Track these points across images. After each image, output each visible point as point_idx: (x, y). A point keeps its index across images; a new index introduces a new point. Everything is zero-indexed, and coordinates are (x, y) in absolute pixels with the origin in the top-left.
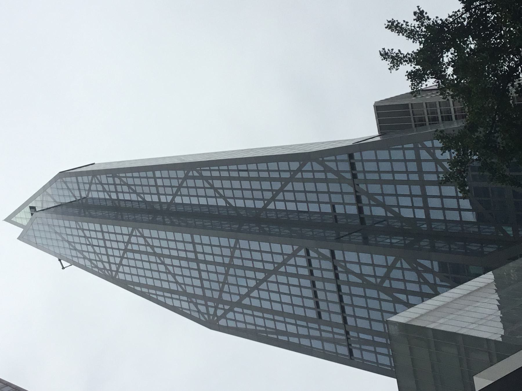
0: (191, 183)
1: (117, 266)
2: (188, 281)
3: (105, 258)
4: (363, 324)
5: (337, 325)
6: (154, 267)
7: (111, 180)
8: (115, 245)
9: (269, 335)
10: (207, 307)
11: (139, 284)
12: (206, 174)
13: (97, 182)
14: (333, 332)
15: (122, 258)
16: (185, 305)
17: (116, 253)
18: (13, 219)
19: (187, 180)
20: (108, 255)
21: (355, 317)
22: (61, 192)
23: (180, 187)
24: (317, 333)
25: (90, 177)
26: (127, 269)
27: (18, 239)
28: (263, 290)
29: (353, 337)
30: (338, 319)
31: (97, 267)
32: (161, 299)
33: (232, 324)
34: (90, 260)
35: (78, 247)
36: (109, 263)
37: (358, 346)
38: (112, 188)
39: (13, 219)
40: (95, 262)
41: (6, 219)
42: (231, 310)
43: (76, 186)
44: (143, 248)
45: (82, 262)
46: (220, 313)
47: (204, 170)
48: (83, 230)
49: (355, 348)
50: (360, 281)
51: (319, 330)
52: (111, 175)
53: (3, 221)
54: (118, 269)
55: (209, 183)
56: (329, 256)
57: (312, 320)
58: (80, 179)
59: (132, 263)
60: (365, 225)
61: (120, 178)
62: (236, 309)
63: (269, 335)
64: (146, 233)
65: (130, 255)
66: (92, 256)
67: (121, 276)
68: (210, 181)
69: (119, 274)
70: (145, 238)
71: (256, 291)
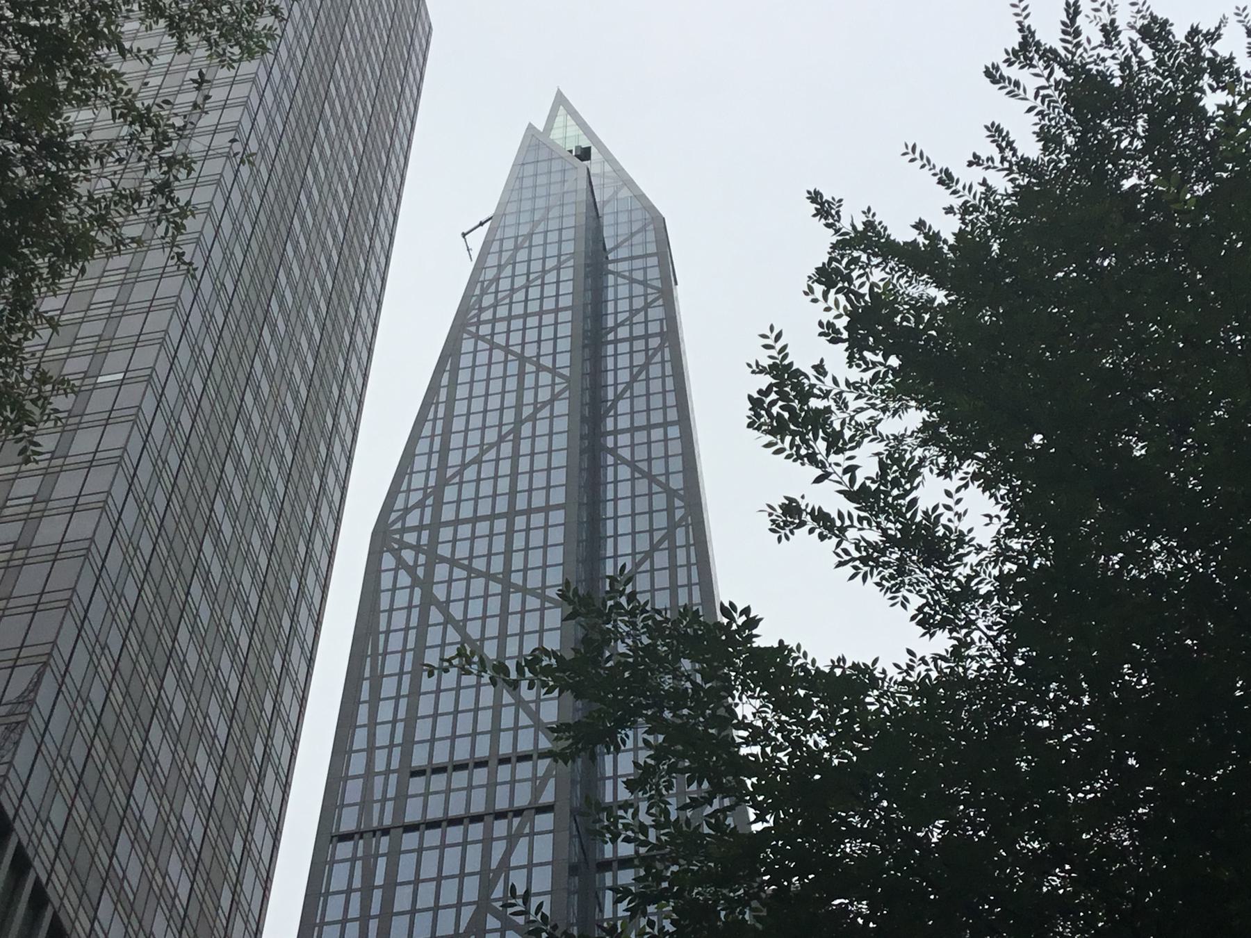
0: (660, 501)
1: (489, 337)
2: (468, 491)
3: (502, 311)
4: (406, 869)
5: (400, 810)
6: (492, 419)
7: (654, 328)
8: (532, 335)
9: (369, 659)
10: (419, 528)
11: (453, 384)
12: (680, 535)
13: (650, 298)
14: (384, 799)
15: (507, 349)
16: (418, 481)
17: (516, 338)
18: (562, 110)
19: (664, 495)
20: (509, 318)
21: (420, 850)
22: (623, 218)
23: (652, 479)
24: (380, 766)
25: (658, 284)
26: (482, 358)
27: (530, 124)
28: (395, 578)
29: (378, 843)
30: (413, 814)
31: (484, 292)
32: (427, 430)
33: (386, 580)
34: (497, 279)
35: (522, 255)
36: (494, 321)
37: (360, 854)
38: (639, 330)
39: (562, 110)
40: (493, 289)
41: (561, 94)
42: (416, 582)
43: (638, 251)
44: (528, 397)
45: (492, 260)
46: (408, 555)
47: (687, 533)
48: (558, 268)
49: (356, 848)
50: (494, 865)
51: (388, 772)
52: (665, 330)
53: (822, 361)
54: (483, 338)
55: (661, 541)
56: (540, 802)
57: (407, 755)
58: (653, 261)
59: (497, 370)
60: (598, 872)
61: (661, 348)
62: (418, 591)
63: (369, 659)
64: (562, 407)
65: (513, 368)
66: (505, 284)
67: (468, 345)
68: (665, 545)
69: (473, 340)
70: (551, 402)
71: (441, 619)
